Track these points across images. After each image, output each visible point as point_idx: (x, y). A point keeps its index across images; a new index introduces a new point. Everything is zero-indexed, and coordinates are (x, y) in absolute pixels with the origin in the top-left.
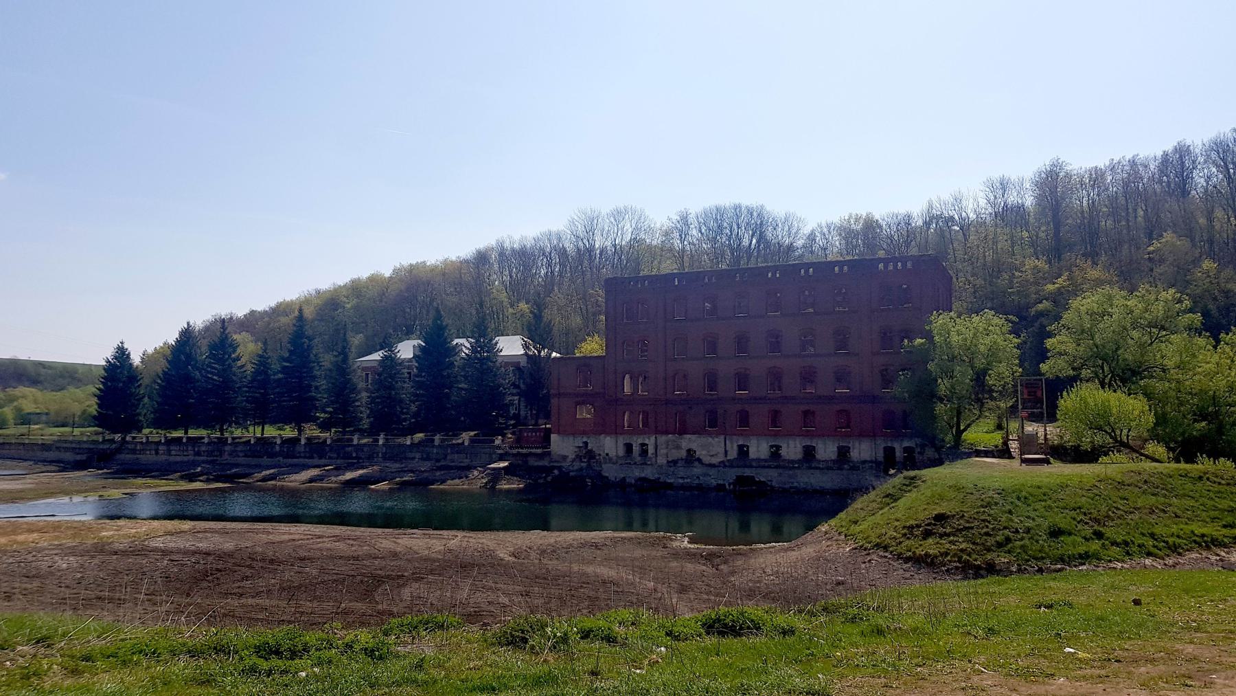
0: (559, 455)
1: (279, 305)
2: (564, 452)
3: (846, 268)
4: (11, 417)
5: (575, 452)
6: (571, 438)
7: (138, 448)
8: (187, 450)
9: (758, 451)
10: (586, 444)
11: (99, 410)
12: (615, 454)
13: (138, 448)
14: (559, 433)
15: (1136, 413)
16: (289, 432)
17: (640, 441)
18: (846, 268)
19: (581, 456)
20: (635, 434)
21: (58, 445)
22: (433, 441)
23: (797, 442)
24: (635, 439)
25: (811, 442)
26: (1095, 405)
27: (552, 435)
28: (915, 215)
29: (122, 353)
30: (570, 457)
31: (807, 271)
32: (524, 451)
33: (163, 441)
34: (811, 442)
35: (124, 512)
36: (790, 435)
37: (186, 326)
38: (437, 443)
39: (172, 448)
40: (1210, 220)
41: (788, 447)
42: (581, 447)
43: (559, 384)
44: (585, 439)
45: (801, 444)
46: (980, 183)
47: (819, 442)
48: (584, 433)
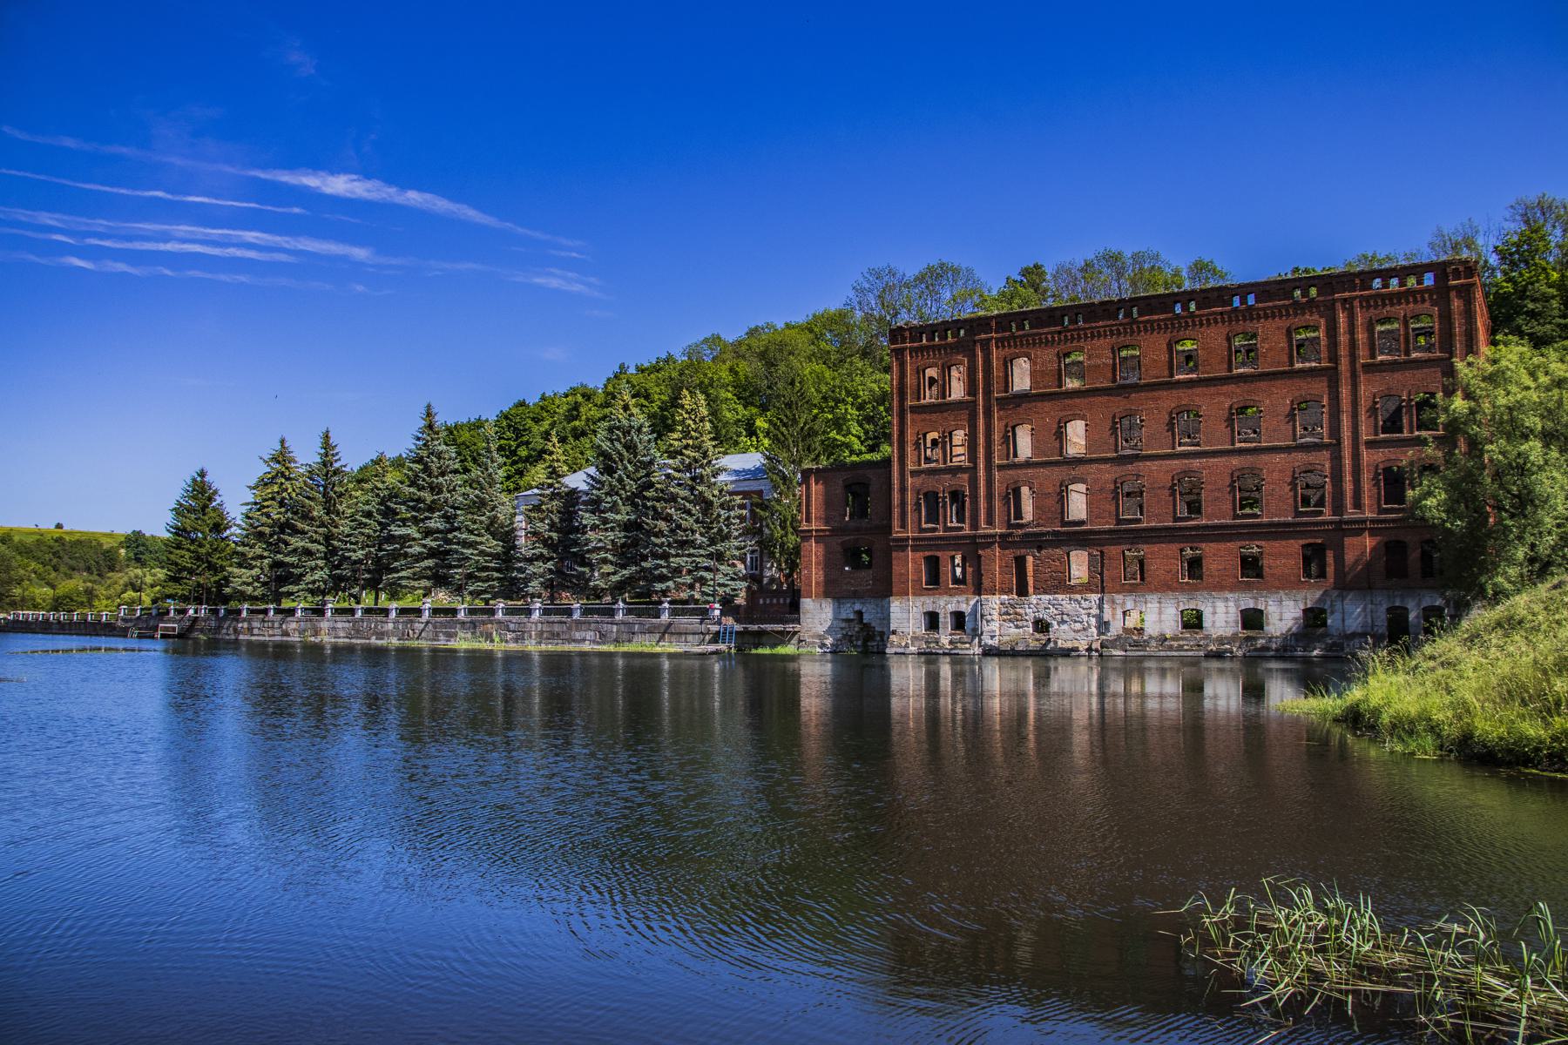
10: (860, 614)
44: (857, 607)
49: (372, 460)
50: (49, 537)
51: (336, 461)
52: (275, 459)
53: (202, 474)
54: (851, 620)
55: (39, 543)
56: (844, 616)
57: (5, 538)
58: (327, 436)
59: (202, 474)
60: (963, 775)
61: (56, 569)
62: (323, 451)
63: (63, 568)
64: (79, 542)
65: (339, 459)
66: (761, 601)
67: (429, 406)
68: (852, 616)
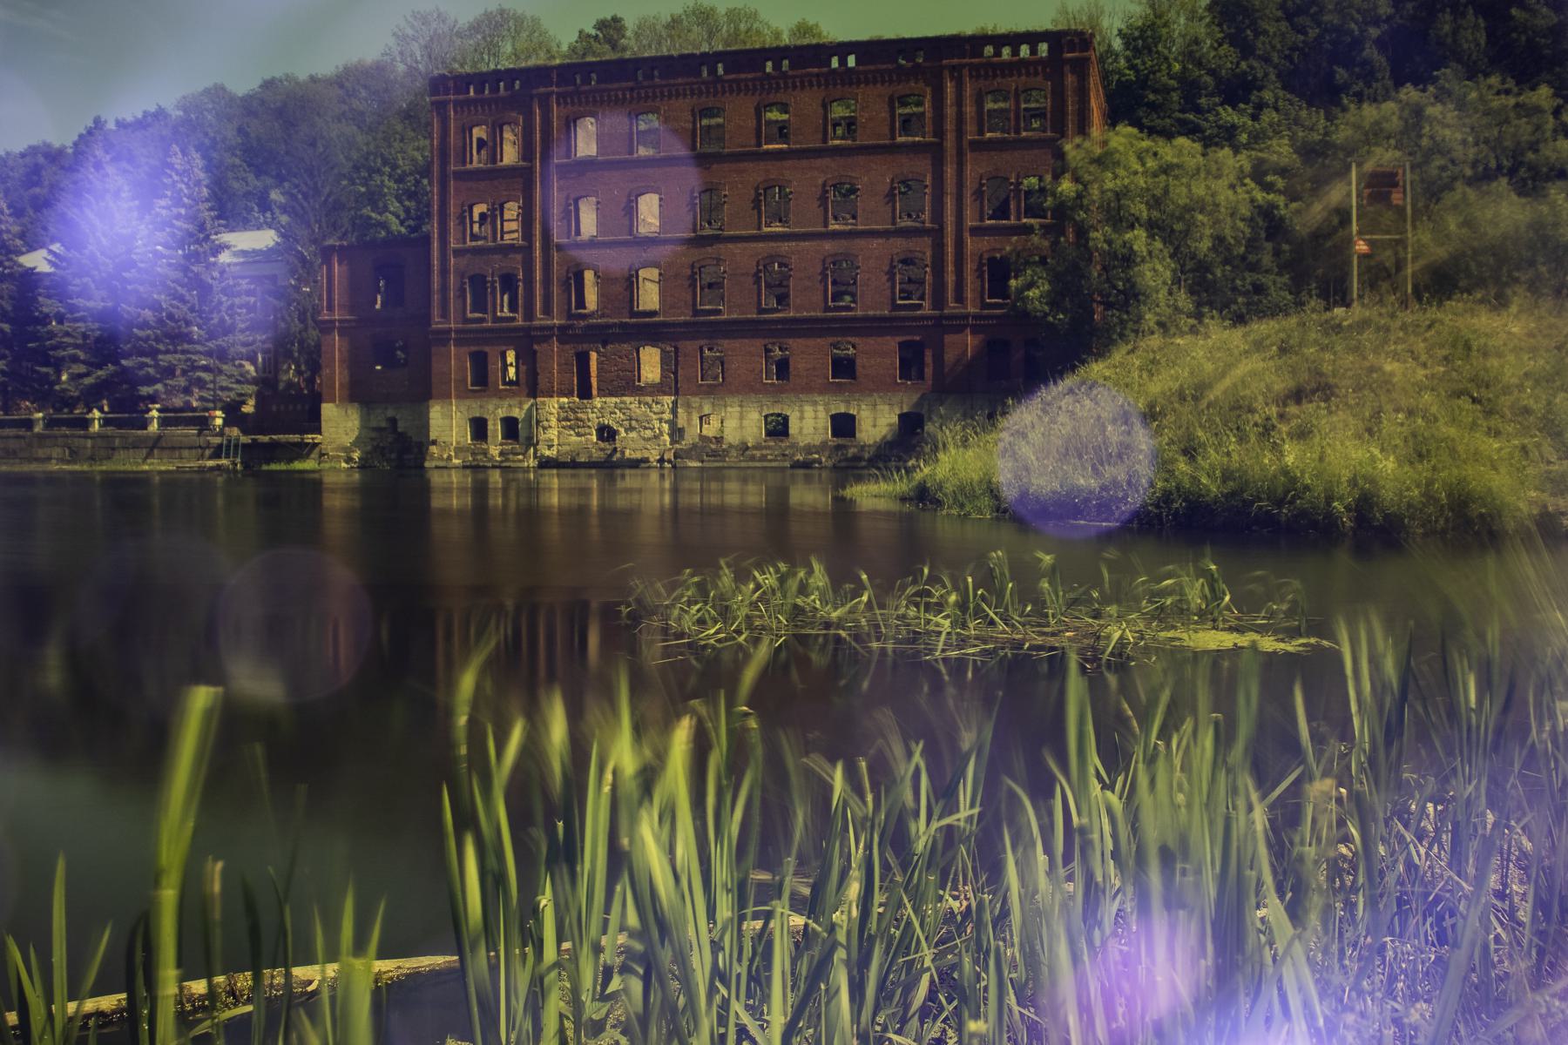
1: (348, 71)
4: (1490, 344)
5: (372, 439)
9: (741, 427)
17: (501, 413)
19: (384, 448)
23: (821, 408)
25: (848, 407)
26: (1534, 350)
27: (324, 406)
28: (630, 24)
32: (265, 439)
34: (848, 407)
35: (1470, 471)
36: (808, 389)
41: (802, 418)
42: (385, 429)
44: (390, 413)
45: (827, 411)
47: (863, 407)
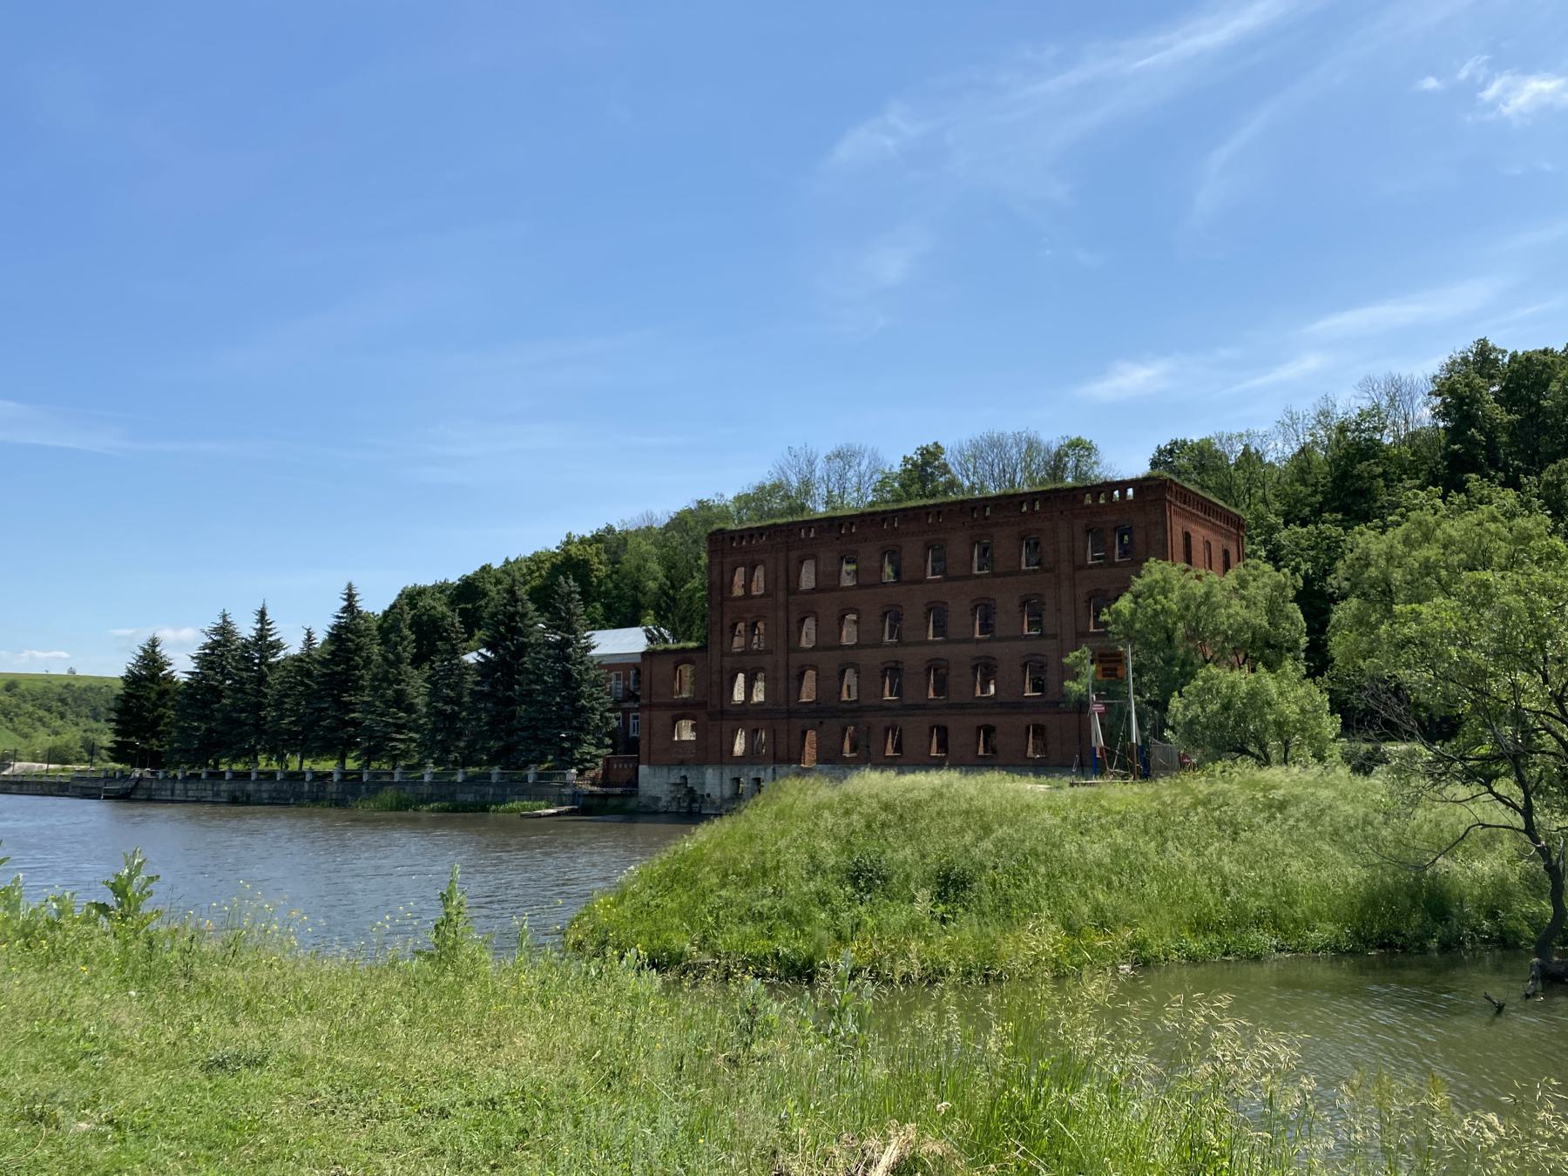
0: (650, 796)
2: (656, 792)
3: (1130, 492)
6: (665, 771)
7: (154, 786)
8: (205, 790)
10: (685, 778)
11: (119, 739)
12: (718, 794)
13: (154, 786)
14: (649, 764)
15: (1094, 988)
16: (328, 765)
17: (753, 775)
18: (1130, 492)
20: (745, 764)
21: (76, 783)
22: (489, 776)
24: (746, 770)
29: (152, 659)
30: (663, 800)
31: (1123, 494)
33: (180, 778)
37: (220, 621)
38: (494, 779)
39: (189, 786)
40: (113, 720)
43: (651, 689)
44: (683, 773)
46: (1354, 387)
48: (682, 763)
49: (1311, 674)
50: (56, 683)
51: (271, 635)
52: (216, 631)
53: (154, 643)
54: (679, 784)
55: (45, 692)
56: (672, 781)
57: (11, 686)
58: (262, 614)
59: (154, 643)
60: (425, 710)
61: (62, 716)
62: (259, 626)
63: (70, 716)
64: (89, 689)
65: (275, 634)
66: (615, 766)
67: (350, 587)
68: (678, 781)
